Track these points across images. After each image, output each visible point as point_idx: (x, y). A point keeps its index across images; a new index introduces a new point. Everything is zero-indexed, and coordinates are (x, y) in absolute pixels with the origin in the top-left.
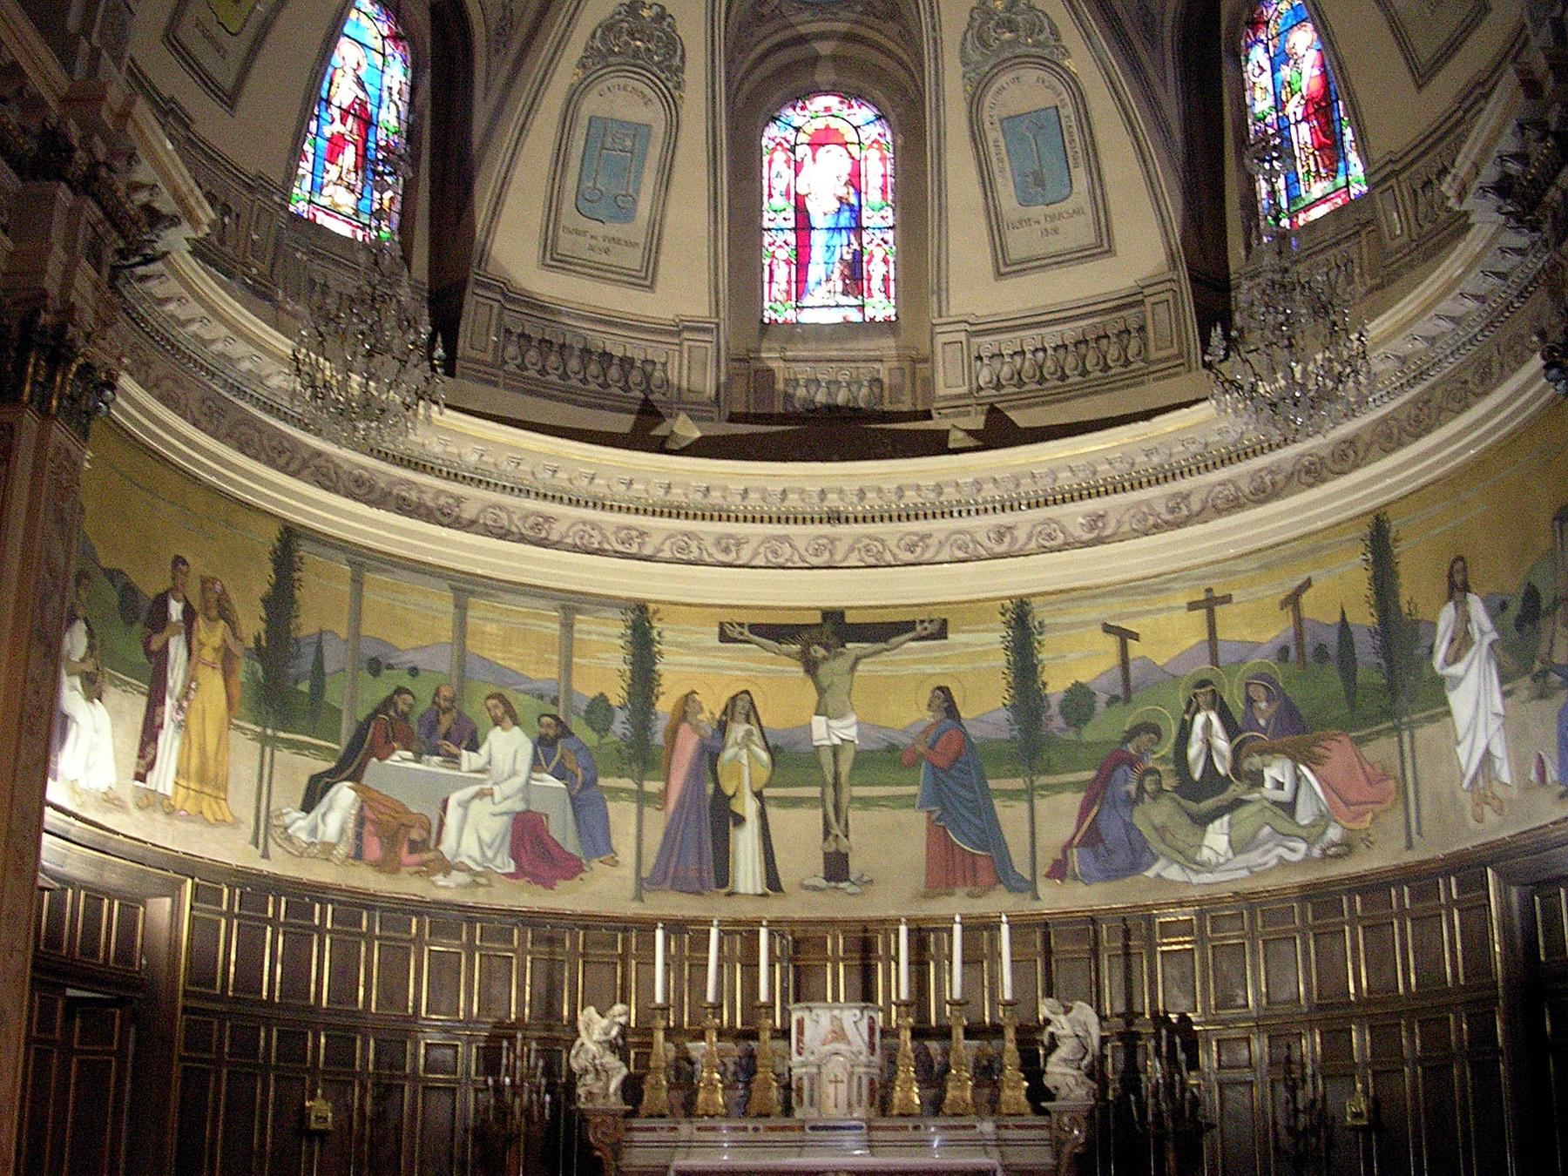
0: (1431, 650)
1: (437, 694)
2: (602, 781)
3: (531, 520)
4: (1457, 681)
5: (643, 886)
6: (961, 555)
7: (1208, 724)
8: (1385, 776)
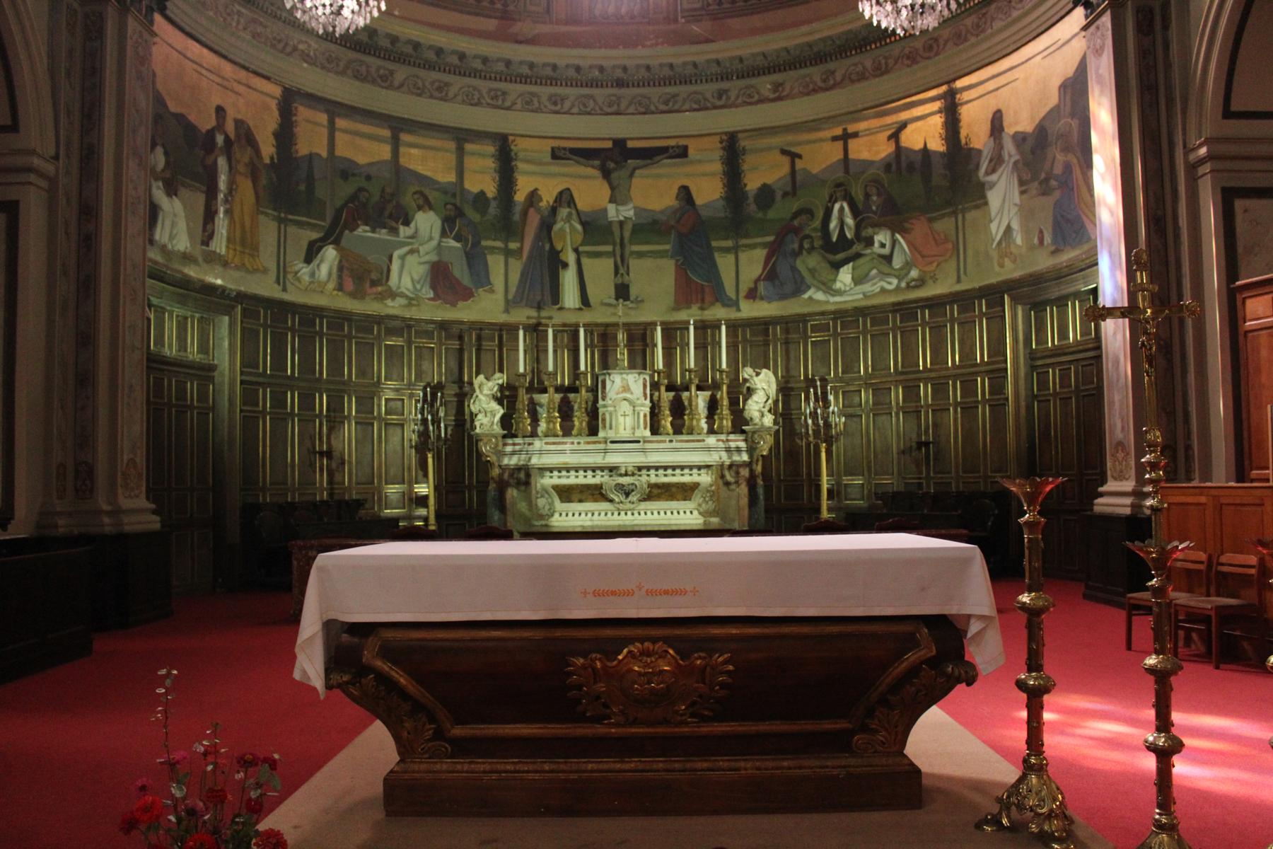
0: (978, 167)
1: (383, 191)
2: (484, 243)
4: (992, 185)
5: (509, 305)
6: (695, 106)
8: (946, 240)
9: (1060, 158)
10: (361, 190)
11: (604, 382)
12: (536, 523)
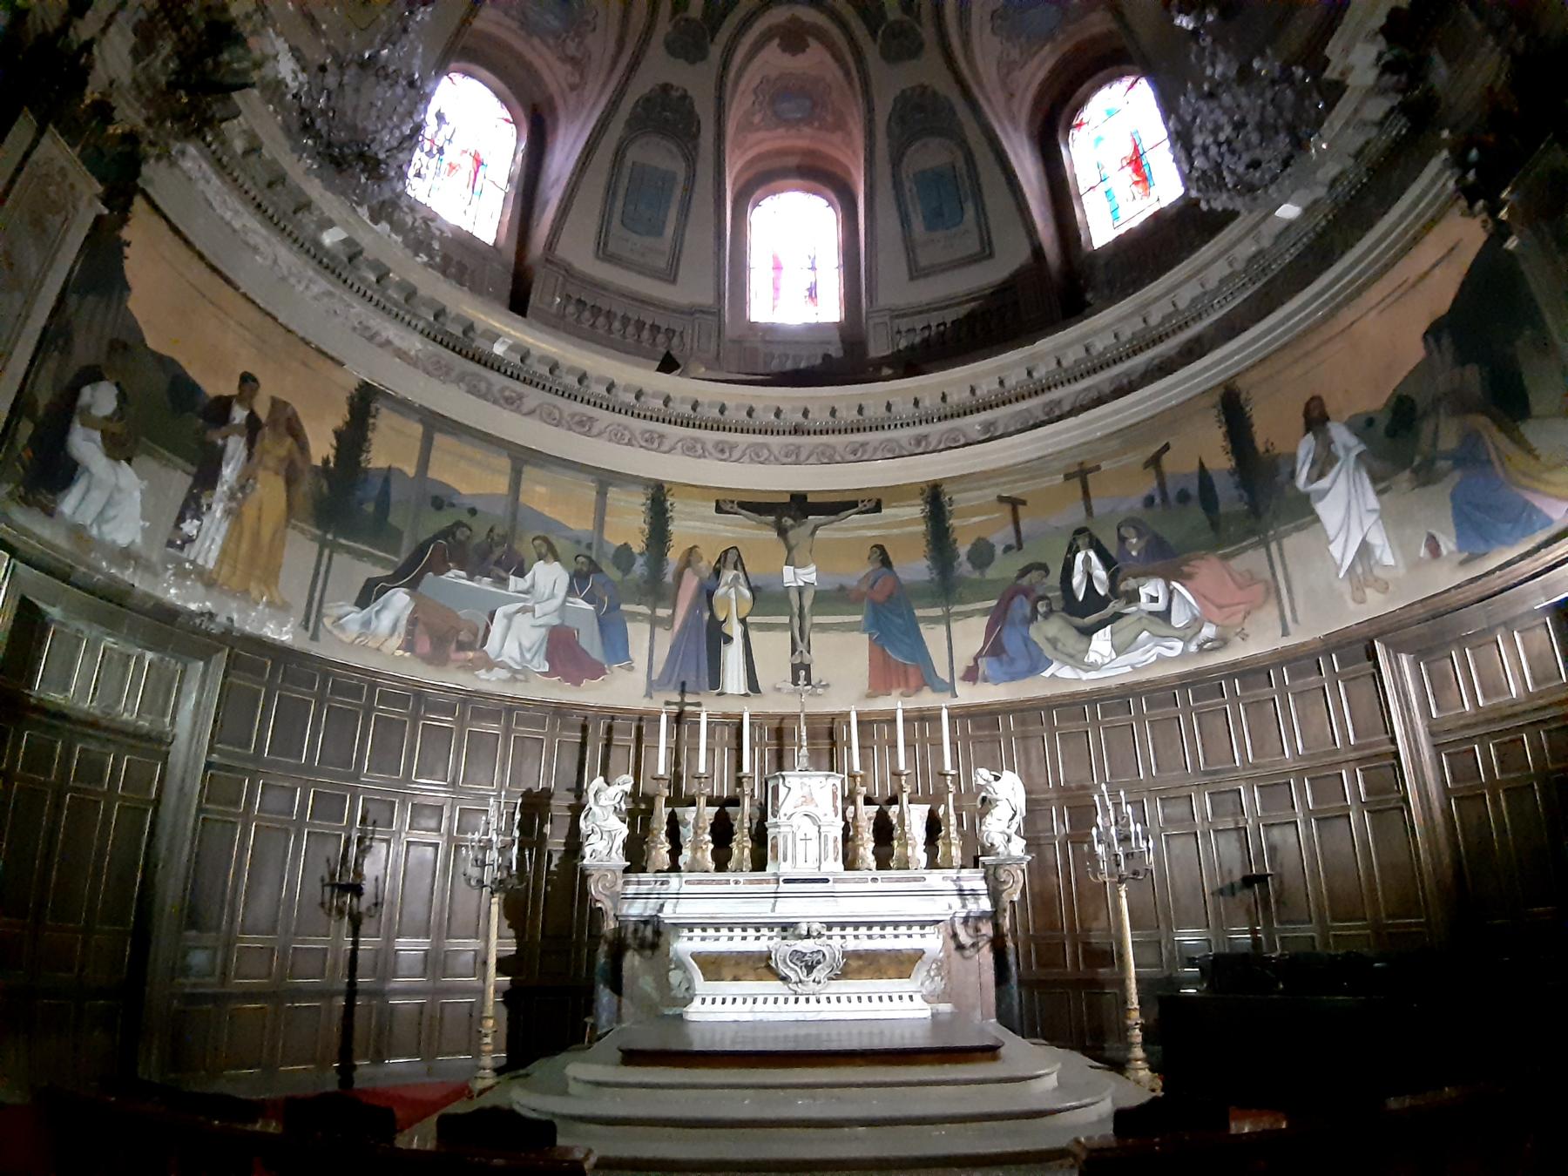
0: (1293, 475)
1: (491, 530)
2: (623, 607)
4: (1323, 494)
5: (652, 687)
7: (1087, 560)
10: (459, 524)
11: (776, 789)
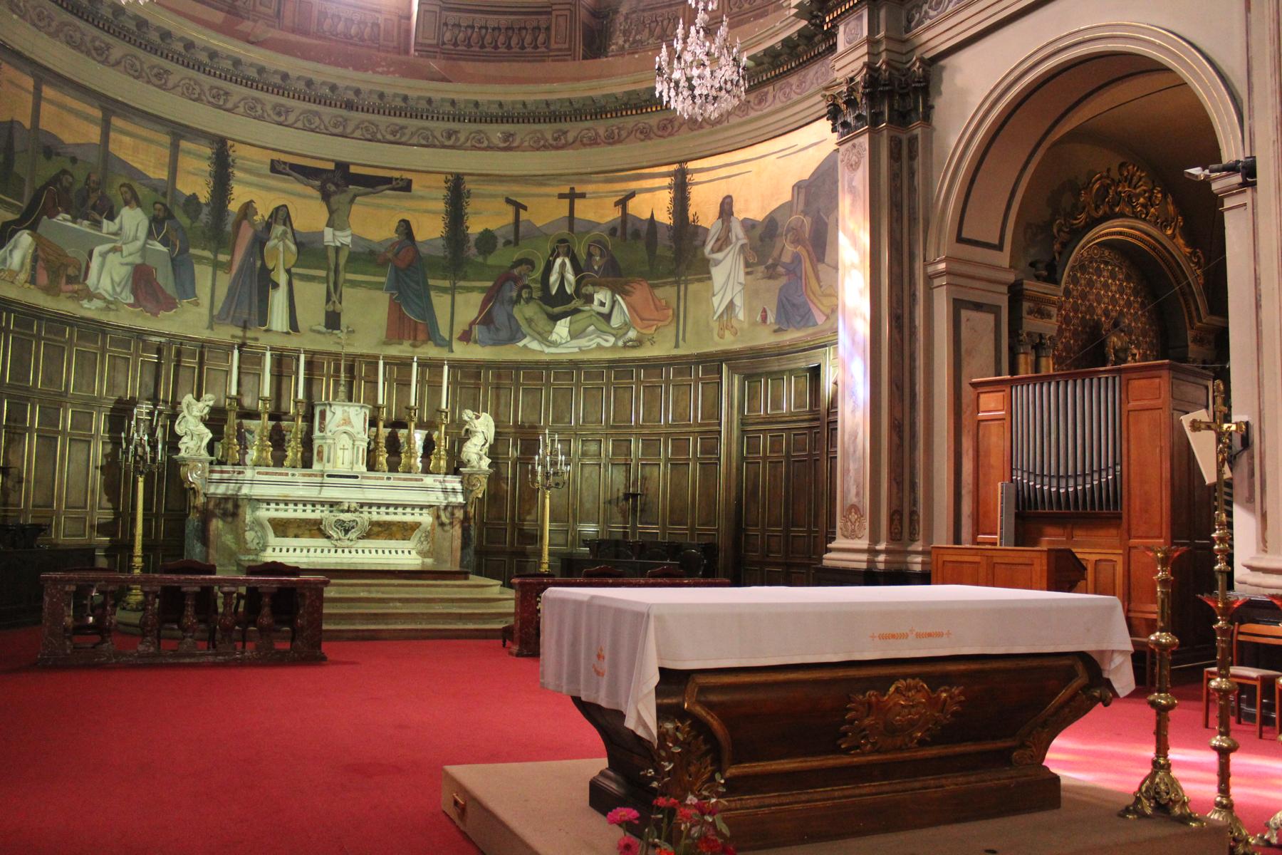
0: (704, 243)
1: (89, 177)
2: (192, 251)
3: (155, 70)
4: (717, 263)
6: (424, 142)
7: (563, 264)
8: (667, 307)
9: (790, 249)
11: (323, 414)
12: (243, 558)
